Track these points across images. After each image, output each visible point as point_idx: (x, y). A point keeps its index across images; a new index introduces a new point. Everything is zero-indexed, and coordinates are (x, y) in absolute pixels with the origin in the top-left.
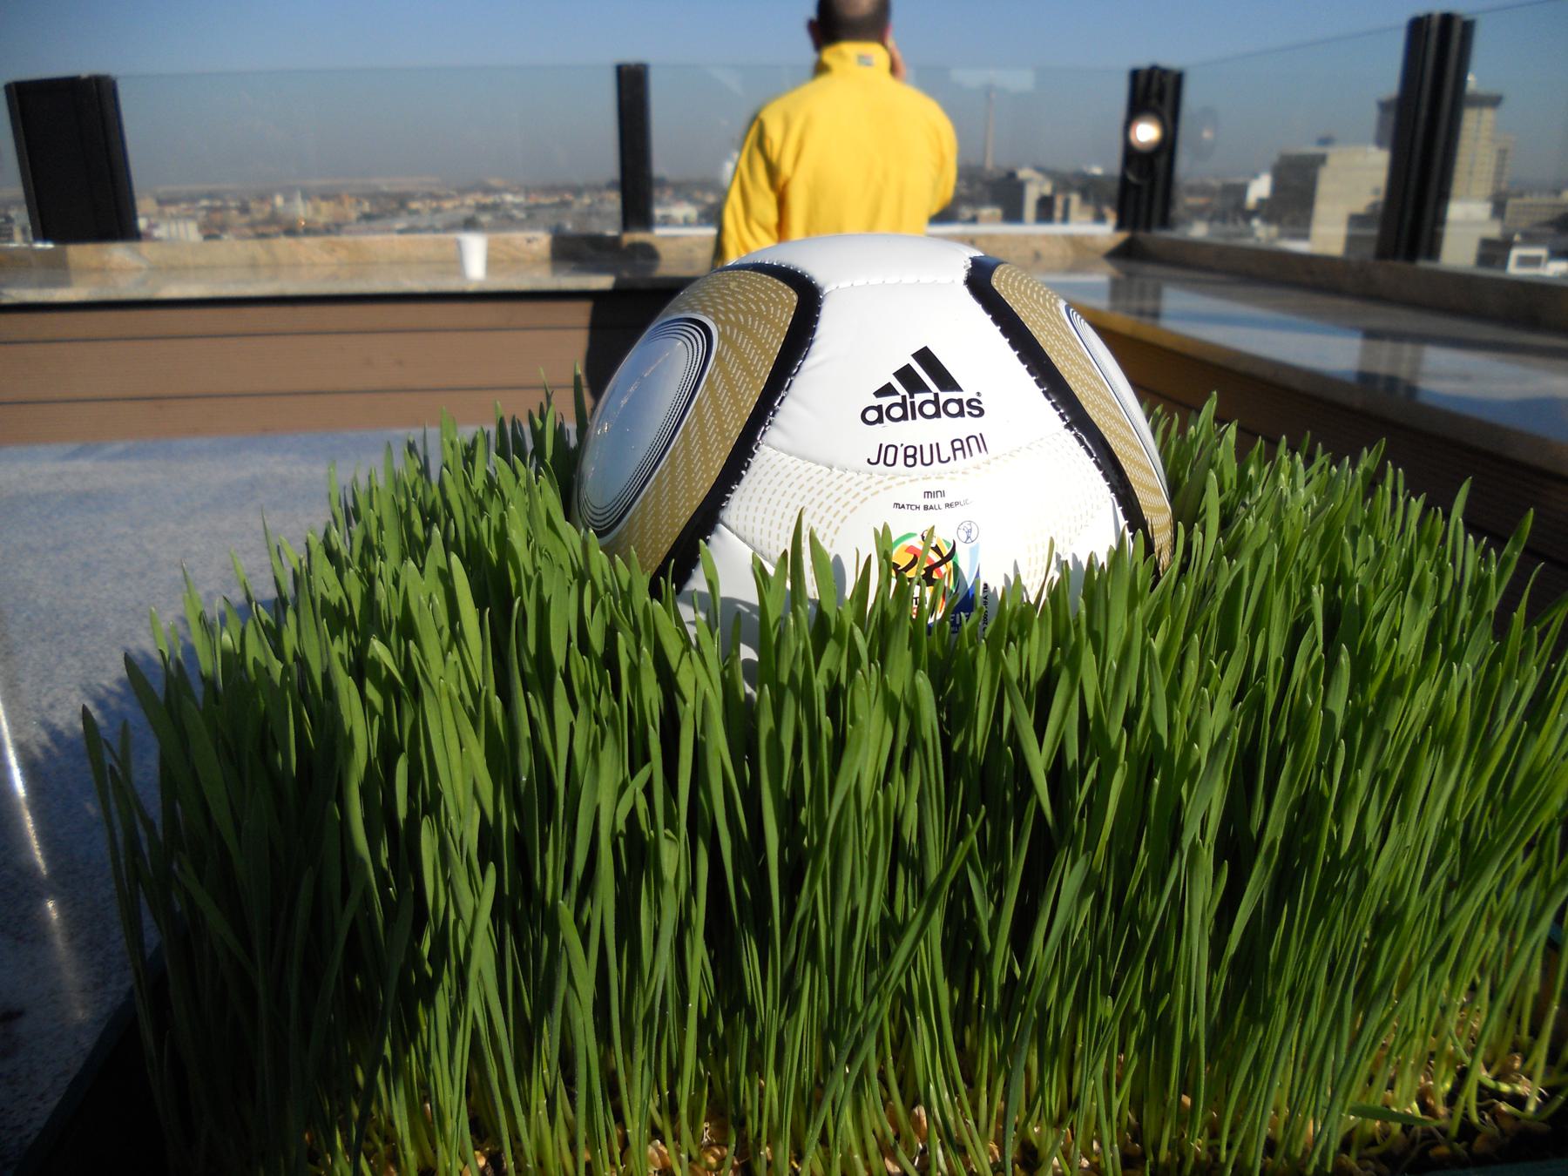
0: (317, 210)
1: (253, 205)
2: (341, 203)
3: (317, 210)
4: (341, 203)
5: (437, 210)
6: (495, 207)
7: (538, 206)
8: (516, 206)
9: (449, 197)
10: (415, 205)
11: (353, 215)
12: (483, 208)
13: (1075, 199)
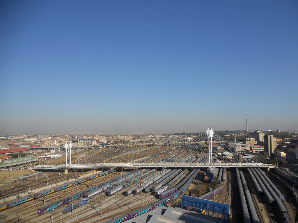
0: (125, 138)
1: (114, 137)
2: (129, 136)
3: (125, 138)
4: (129, 136)
5: (145, 138)
6: (155, 137)
7: (162, 137)
8: (158, 137)
9: (147, 136)
10: (141, 137)
11: (131, 138)
12: (153, 138)
13: (272, 136)
